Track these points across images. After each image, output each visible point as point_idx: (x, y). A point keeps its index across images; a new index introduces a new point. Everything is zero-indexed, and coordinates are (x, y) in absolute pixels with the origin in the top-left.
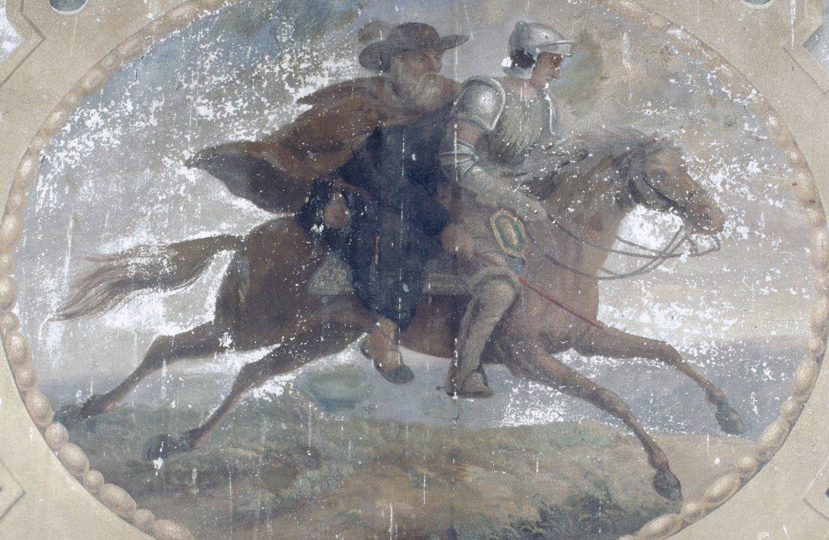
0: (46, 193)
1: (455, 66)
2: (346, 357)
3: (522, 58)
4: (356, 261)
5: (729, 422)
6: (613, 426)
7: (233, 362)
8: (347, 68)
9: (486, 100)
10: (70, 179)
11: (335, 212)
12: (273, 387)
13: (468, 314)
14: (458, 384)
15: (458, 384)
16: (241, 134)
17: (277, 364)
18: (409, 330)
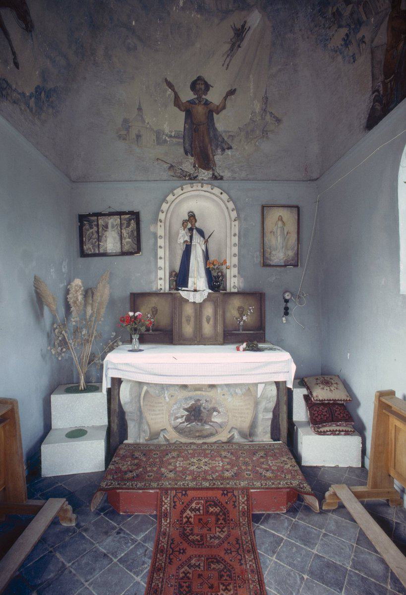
0: (172, 412)
1: (201, 402)
2: (194, 423)
3: (206, 401)
4: (194, 416)
5: (221, 428)
6: (213, 428)
7: (186, 424)
8: (193, 402)
9: (204, 404)
10: (173, 411)
11: (193, 413)
12: (189, 426)
13: (334, 428)
14: (202, 425)
15: (202, 425)
16: (186, 407)
17: (189, 424)
18: (198, 421)
